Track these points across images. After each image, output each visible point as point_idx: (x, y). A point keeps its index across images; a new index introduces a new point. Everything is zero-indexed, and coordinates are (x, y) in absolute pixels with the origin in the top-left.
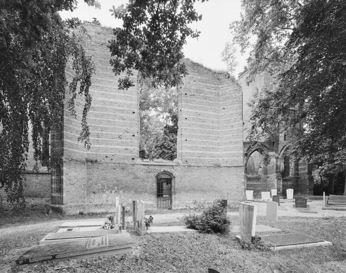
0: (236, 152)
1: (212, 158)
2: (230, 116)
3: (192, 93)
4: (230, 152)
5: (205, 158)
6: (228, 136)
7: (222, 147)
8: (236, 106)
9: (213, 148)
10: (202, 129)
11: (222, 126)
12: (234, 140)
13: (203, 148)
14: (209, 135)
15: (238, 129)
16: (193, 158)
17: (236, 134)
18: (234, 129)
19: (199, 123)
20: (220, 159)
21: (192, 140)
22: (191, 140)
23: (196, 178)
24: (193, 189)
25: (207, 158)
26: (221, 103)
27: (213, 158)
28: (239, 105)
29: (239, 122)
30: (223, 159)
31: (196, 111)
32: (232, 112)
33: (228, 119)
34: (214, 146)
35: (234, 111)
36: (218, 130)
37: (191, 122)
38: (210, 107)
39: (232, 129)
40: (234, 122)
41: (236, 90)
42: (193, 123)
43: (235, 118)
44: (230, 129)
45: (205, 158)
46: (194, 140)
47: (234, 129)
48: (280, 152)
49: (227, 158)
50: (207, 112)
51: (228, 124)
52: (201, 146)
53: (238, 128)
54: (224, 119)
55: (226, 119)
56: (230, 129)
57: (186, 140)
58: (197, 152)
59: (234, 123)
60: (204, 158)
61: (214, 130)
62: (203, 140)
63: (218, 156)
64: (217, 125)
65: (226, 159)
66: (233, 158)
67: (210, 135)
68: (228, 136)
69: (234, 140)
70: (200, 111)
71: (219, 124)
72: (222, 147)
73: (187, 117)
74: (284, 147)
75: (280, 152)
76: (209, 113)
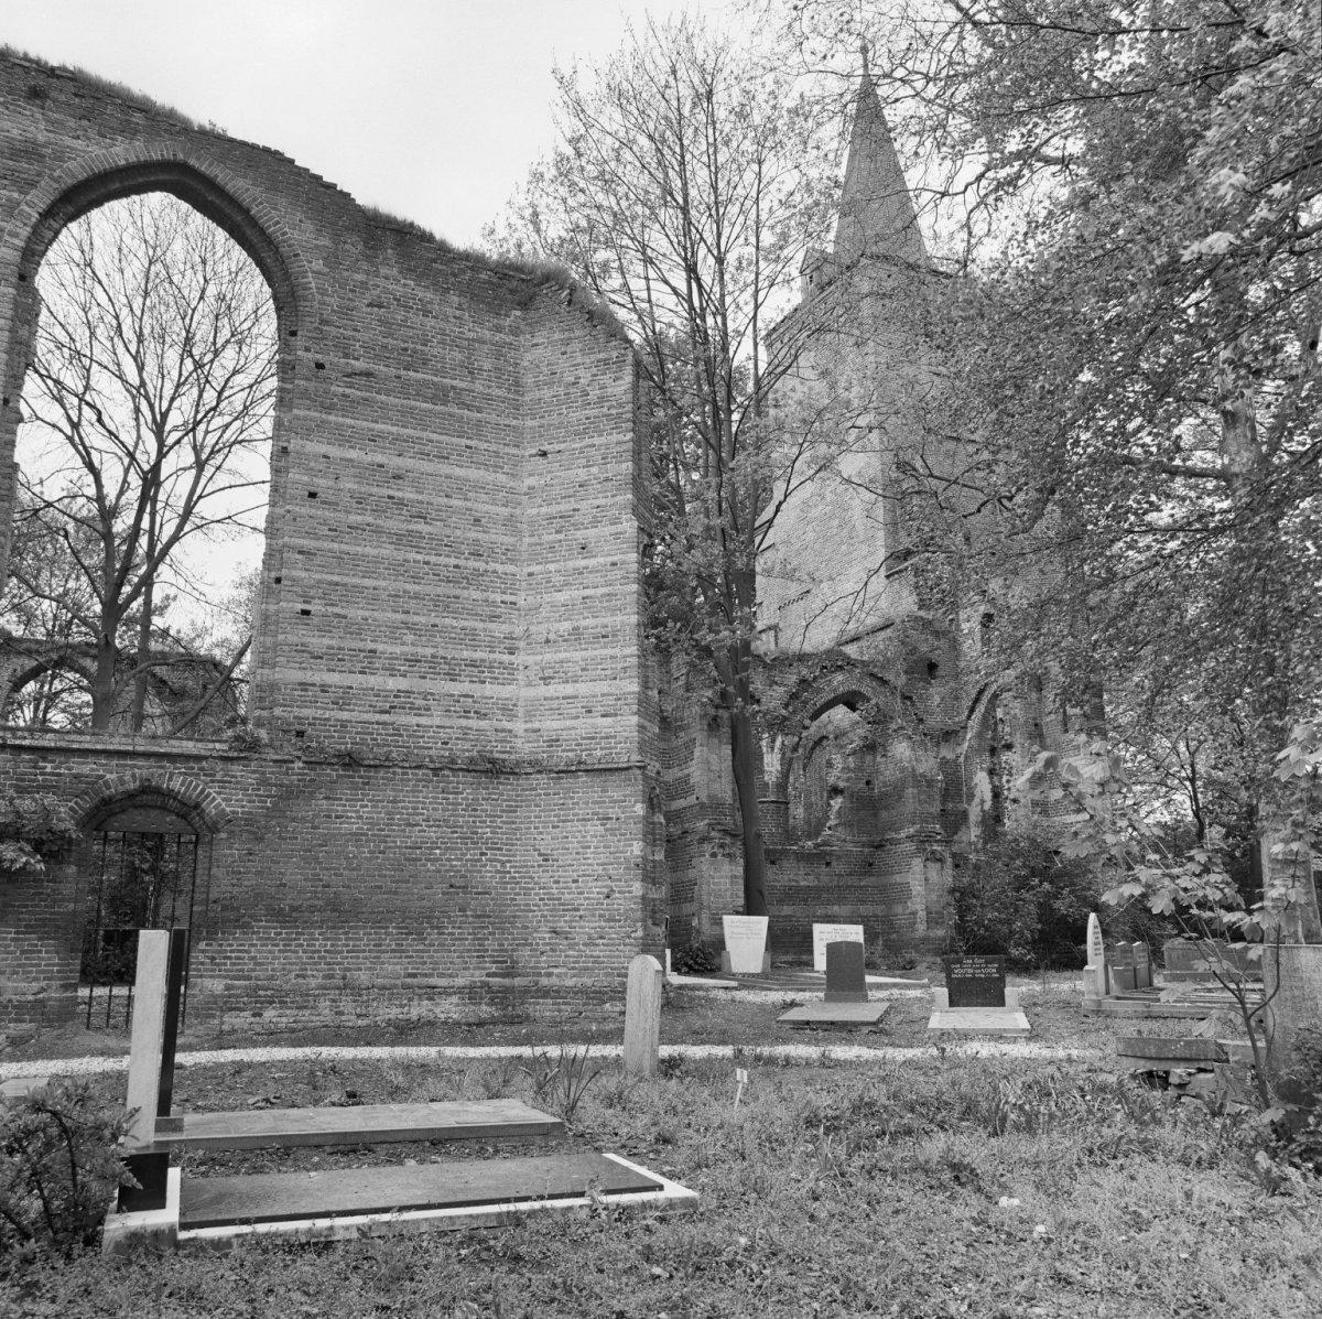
0: (602, 687)
1: (464, 722)
2: (571, 491)
3: (360, 365)
4: (569, 689)
5: (423, 721)
6: (561, 597)
7: (530, 660)
8: (603, 440)
9: (473, 664)
10: (412, 556)
11: (530, 545)
12: (590, 622)
13: (414, 661)
14: (451, 590)
15: (614, 564)
16: (345, 715)
17: (600, 591)
18: (592, 562)
19: (394, 525)
20: (519, 726)
21: (343, 612)
22: (338, 615)
23: (356, 837)
24: (334, 906)
25: (437, 721)
26: (530, 423)
27: (473, 723)
28: (615, 437)
29: (619, 528)
30: (536, 725)
31: (379, 458)
32: (582, 474)
33: (565, 507)
34: (479, 655)
35: (594, 470)
36: (510, 568)
37: (342, 515)
38: (464, 442)
39: (583, 563)
40: (595, 522)
41: (606, 362)
42: (354, 519)
43: (598, 502)
44: (571, 564)
45: (423, 721)
46: (356, 613)
47: (592, 562)
48: (969, 717)
49: (555, 725)
50: (445, 469)
51: (561, 536)
52: (398, 650)
53: (615, 559)
54: (544, 510)
55: (554, 509)
56: (571, 564)
57: (306, 613)
58: (373, 681)
59: (592, 532)
60: (415, 720)
61: (481, 565)
62: (416, 619)
63: (508, 710)
64: (501, 539)
65: (550, 725)
66: (584, 725)
67: (458, 592)
68: (561, 597)
69: (590, 622)
70: (399, 461)
71: (518, 533)
72: (530, 660)
73: (322, 484)
74: (981, 692)
75: (969, 717)
76: (458, 472)
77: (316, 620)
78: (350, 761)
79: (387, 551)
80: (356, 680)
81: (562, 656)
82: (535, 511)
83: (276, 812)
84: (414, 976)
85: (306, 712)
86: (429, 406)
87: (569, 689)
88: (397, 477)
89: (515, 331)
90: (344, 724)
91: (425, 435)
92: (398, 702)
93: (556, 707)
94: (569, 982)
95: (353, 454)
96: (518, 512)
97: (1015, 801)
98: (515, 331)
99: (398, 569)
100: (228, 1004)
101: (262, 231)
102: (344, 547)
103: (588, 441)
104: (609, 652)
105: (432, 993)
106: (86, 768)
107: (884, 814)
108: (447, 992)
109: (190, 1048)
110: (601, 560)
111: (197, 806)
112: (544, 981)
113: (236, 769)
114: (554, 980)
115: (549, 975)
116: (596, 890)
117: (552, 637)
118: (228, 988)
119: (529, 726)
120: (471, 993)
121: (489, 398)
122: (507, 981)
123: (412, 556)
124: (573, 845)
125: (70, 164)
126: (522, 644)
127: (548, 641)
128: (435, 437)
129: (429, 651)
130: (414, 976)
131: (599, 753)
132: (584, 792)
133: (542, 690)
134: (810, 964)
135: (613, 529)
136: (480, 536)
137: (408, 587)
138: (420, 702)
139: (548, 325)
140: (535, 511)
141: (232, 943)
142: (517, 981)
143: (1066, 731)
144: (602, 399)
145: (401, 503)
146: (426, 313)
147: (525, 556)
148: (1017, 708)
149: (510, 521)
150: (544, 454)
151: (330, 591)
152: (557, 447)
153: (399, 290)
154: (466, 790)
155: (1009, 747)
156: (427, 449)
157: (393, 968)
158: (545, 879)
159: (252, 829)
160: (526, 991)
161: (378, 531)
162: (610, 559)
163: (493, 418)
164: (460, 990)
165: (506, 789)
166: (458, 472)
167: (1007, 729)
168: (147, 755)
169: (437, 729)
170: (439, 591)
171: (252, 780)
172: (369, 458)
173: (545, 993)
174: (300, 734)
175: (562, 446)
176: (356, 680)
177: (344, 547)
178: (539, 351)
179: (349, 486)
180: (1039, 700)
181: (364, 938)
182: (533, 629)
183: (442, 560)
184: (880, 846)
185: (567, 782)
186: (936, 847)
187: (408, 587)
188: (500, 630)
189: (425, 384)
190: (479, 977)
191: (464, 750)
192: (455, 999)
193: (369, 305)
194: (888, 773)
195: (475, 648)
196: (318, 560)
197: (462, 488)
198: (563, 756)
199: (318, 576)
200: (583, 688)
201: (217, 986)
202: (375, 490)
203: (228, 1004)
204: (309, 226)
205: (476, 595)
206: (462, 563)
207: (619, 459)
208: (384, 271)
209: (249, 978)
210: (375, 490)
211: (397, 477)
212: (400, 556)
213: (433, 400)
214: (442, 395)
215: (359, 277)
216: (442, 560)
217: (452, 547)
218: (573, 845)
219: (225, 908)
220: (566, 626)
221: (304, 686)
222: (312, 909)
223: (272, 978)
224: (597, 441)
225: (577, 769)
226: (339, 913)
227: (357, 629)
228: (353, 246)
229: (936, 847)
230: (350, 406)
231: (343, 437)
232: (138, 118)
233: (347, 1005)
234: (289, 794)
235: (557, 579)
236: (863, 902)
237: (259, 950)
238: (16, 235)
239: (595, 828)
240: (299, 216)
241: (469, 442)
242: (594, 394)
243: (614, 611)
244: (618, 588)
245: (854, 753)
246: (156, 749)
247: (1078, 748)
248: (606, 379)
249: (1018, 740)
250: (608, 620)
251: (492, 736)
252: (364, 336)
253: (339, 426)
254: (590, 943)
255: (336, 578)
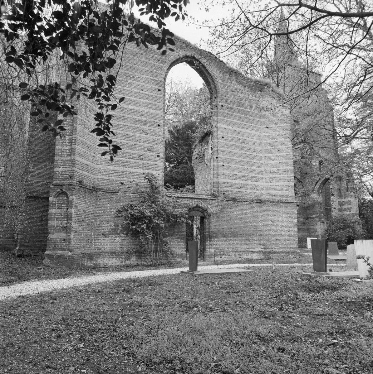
0: (285, 184)
1: (254, 191)
3: (230, 106)
4: (277, 184)
5: (247, 191)
6: (274, 162)
7: (266, 177)
9: (255, 177)
10: (242, 152)
12: (281, 168)
15: (287, 155)
16: (232, 189)
19: (239, 144)
20: (264, 192)
22: (230, 166)
23: (236, 217)
26: (263, 120)
27: (256, 191)
28: (286, 125)
29: (288, 146)
30: (269, 192)
31: (235, 129)
33: (273, 141)
34: (256, 175)
35: (281, 132)
36: (261, 155)
38: (251, 124)
42: (231, 143)
44: (276, 154)
46: (233, 166)
49: (274, 192)
50: (248, 131)
52: (241, 174)
54: (268, 141)
55: (270, 141)
56: (276, 154)
57: (223, 165)
59: (281, 147)
60: (245, 191)
61: (255, 154)
62: (244, 167)
63: (262, 188)
64: (259, 148)
65: (272, 192)
66: (281, 192)
67: (251, 160)
68: (274, 162)
69: (281, 168)
71: (262, 146)
72: (266, 177)
73: (225, 135)
76: (250, 132)
77: (225, 167)
78: (234, 200)
79: (237, 151)
80: (234, 181)
81: (275, 176)
82: (266, 141)
83: (221, 212)
84: (248, 249)
85: (225, 189)
86: (243, 116)
87: (277, 184)
88: (239, 133)
89: (259, 97)
90: (232, 191)
91: (243, 123)
92: (241, 187)
93: (274, 188)
94: (281, 250)
95: (230, 128)
96: (262, 141)
97: (334, 208)
98: (259, 97)
99: (240, 155)
100: (215, 255)
101: (209, 72)
102: (230, 150)
103: (279, 125)
104: (286, 175)
105: (252, 252)
106: (186, 201)
107: (308, 211)
108: (255, 252)
109: (329, 263)
110: (284, 154)
111: (207, 210)
112: (274, 250)
113: (213, 202)
114: (276, 250)
115: (275, 249)
116: (286, 230)
117: (272, 171)
118: (215, 251)
119: (267, 192)
120: (259, 253)
121: (255, 114)
122: (265, 250)
123: (242, 152)
124: (280, 220)
125: (172, 57)
126: (264, 173)
127: (271, 172)
128: (245, 123)
129: (247, 174)
130: (248, 249)
131: (285, 199)
132: (282, 208)
133: (270, 184)
134: (306, 247)
135: (286, 146)
136: (255, 147)
137: (242, 159)
138: (246, 186)
139: (267, 96)
140: (266, 141)
141: (214, 241)
142: (267, 250)
143: (348, 191)
144: (282, 115)
145: (240, 140)
146: (242, 93)
147: (264, 152)
148: (335, 186)
149: (260, 144)
150: (267, 128)
151: (229, 161)
152: (271, 126)
153: (236, 87)
154: (256, 206)
155: (333, 195)
156: (244, 126)
157: (244, 247)
158: (273, 227)
159: (217, 215)
160: (270, 252)
161: (236, 146)
162: (286, 154)
163: (256, 119)
164: (257, 252)
165: (264, 206)
166: (250, 132)
167: (333, 191)
168: (197, 199)
169: (249, 193)
170: (248, 160)
171: (216, 204)
172: (233, 129)
173: (275, 253)
174: (224, 194)
175: (272, 126)
176: (234, 181)
177: (230, 150)
178: (265, 102)
179: (230, 135)
180: (340, 183)
181: (239, 240)
182: (267, 169)
183: (248, 153)
184: (307, 219)
185: (278, 205)
186: (323, 220)
187: (242, 159)
188: (260, 169)
189: (242, 110)
190: (260, 249)
191: (255, 198)
192: (256, 254)
193: (231, 91)
194: (309, 201)
195: (255, 174)
196: (225, 153)
197: (251, 136)
198: (276, 199)
199: (225, 157)
200: (280, 184)
201: (212, 251)
202: (235, 136)
203: (215, 255)
204: (218, 71)
205: (255, 161)
206: (252, 153)
207: (287, 129)
208: (233, 82)
209: (218, 249)
210: (235, 136)
211: (239, 133)
212: (240, 152)
213: (244, 114)
214: (246, 113)
215: (228, 84)
216: (248, 153)
217: (249, 150)
218: (280, 220)
219: (213, 233)
220: (275, 169)
221: (224, 182)
222: (229, 234)
223: (222, 249)
224: (281, 125)
225: (279, 202)
226: (234, 235)
227: (233, 169)
228: (227, 76)
229: (323, 220)
230: (228, 116)
231: (228, 124)
232: (184, 45)
233: (237, 255)
234: (224, 208)
235: (272, 158)
236: (303, 232)
237: (220, 243)
238: (163, 75)
239: (285, 216)
240: (216, 69)
241: (252, 125)
242: (280, 114)
243: (287, 166)
244: (288, 161)
245: (301, 196)
246: (199, 197)
247: (351, 196)
248: (283, 110)
249: (336, 193)
250: (286, 168)
251: (260, 194)
252: (230, 99)
253: (227, 121)
254: (285, 242)
255: (229, 157)
